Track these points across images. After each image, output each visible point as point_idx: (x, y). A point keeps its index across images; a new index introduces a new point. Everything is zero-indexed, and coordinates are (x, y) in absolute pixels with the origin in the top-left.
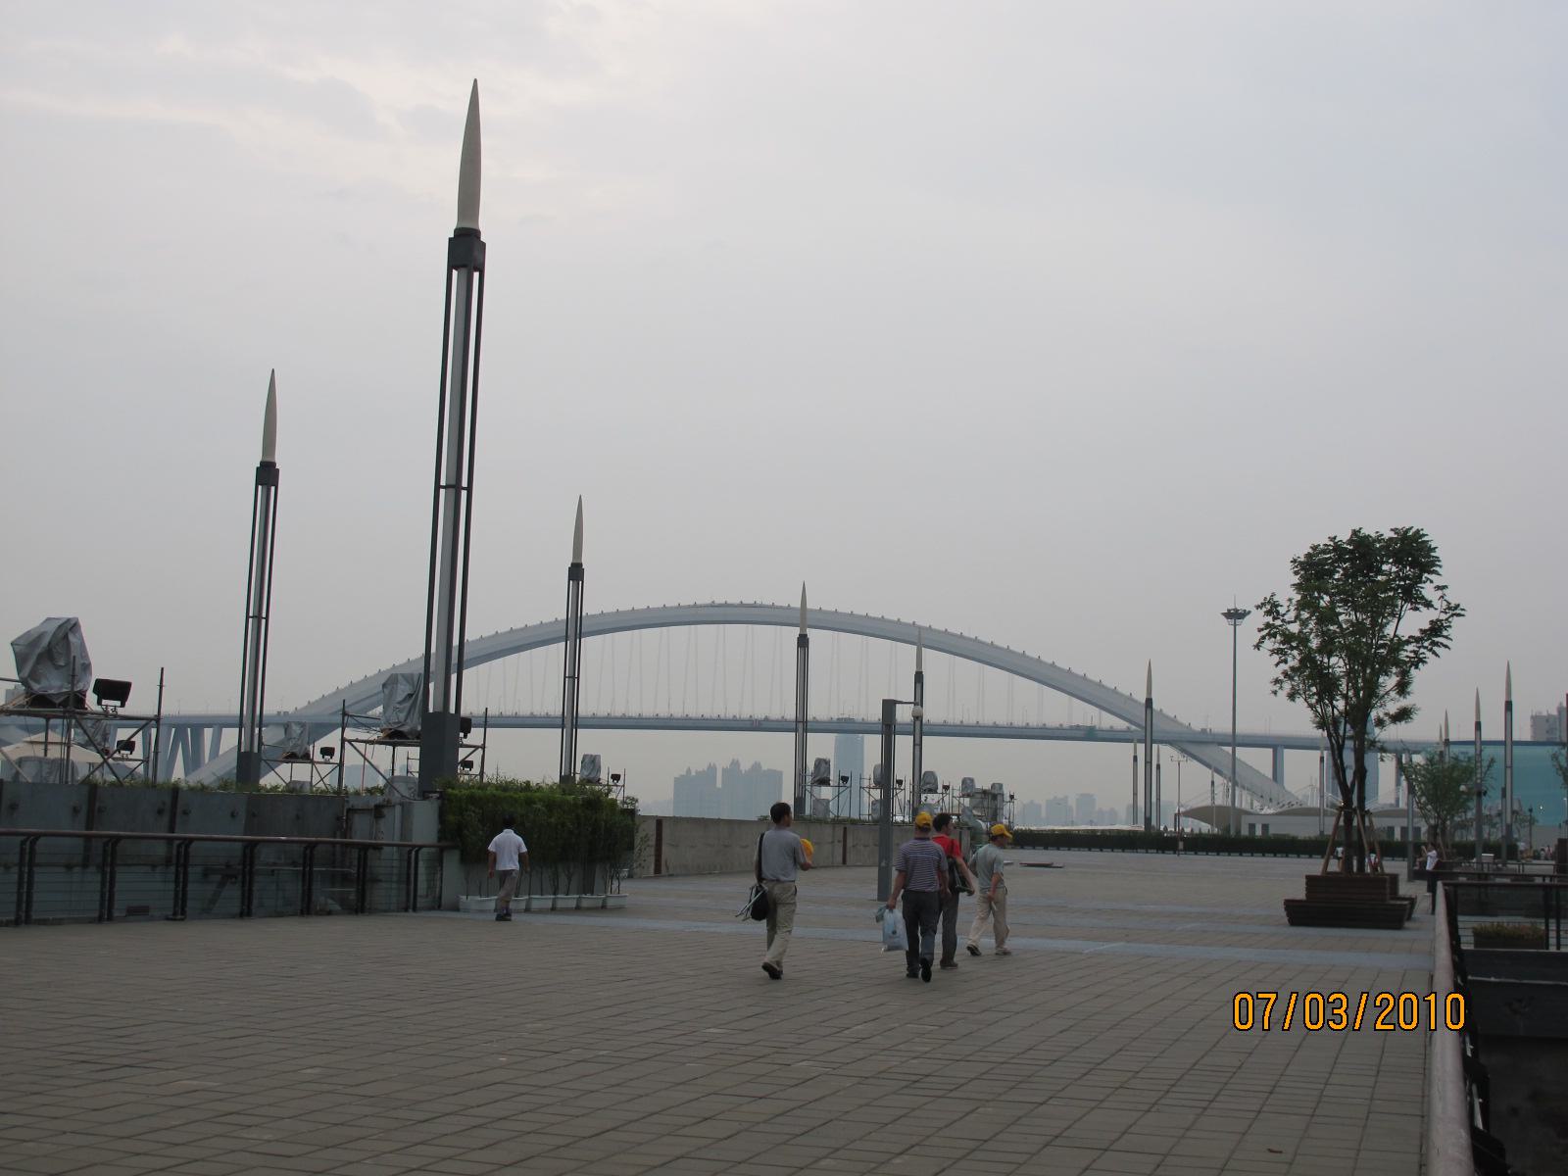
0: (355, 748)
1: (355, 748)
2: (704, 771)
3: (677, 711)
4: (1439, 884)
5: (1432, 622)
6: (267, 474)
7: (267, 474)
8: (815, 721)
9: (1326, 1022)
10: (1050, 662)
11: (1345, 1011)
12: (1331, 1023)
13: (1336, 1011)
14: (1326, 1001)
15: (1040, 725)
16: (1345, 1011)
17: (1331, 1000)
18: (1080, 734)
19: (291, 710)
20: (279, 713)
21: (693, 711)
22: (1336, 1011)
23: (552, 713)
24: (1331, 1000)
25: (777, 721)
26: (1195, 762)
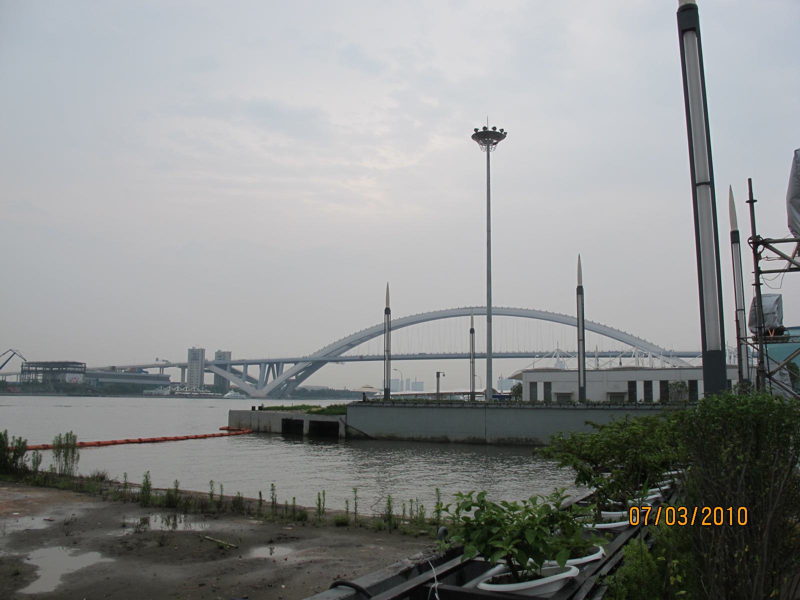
0: (362, 359)
1: (362, 359)
2: (213, 361)
3: (510, 351)
4: (186, 370)
5: (193, 347)
6: (580, 290)
7: (580, 290)
8: (495, 353)
9: (677, 520)
10: (604, 325)
11: (686, 516)
12: (679, 522)
13: (681, 516)
14: (676, 511)
15: (525, 352)
16: (686, 516)
17: (679, 510)
18: (359, 358)
19: (308, 356)
20: (304, 357)
21: (435, 351)
22: (681, 516)
23: (483, 352)
24: (679, 510)
25: (354, 357)
26: (346, 363)
